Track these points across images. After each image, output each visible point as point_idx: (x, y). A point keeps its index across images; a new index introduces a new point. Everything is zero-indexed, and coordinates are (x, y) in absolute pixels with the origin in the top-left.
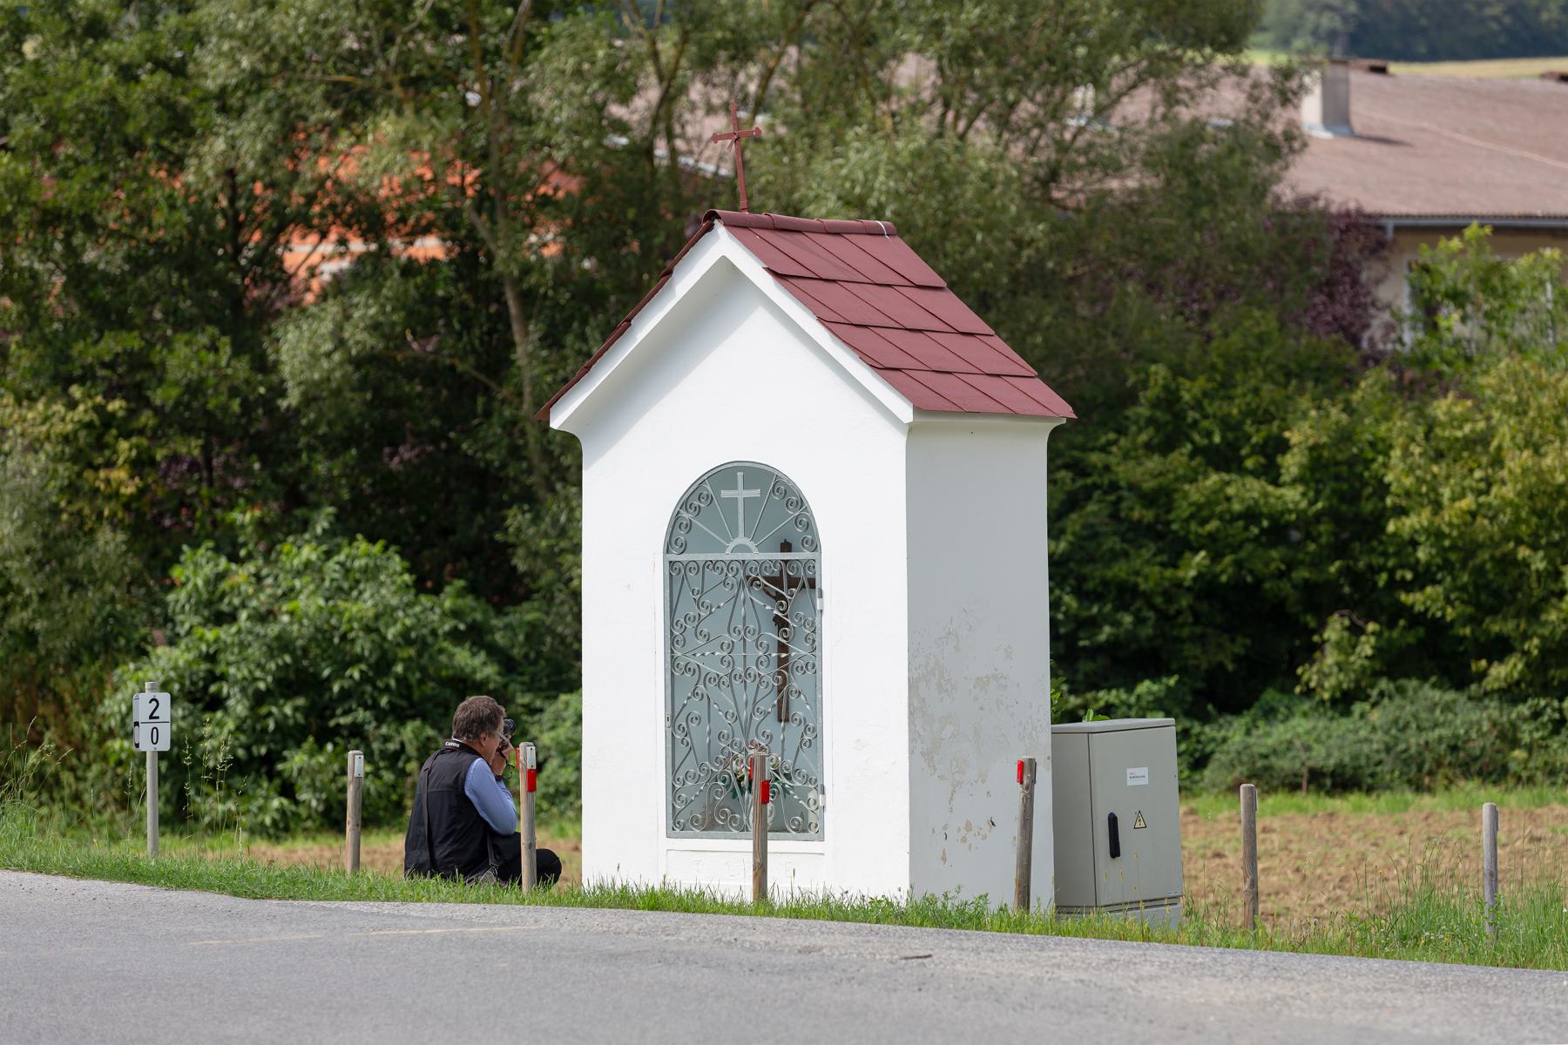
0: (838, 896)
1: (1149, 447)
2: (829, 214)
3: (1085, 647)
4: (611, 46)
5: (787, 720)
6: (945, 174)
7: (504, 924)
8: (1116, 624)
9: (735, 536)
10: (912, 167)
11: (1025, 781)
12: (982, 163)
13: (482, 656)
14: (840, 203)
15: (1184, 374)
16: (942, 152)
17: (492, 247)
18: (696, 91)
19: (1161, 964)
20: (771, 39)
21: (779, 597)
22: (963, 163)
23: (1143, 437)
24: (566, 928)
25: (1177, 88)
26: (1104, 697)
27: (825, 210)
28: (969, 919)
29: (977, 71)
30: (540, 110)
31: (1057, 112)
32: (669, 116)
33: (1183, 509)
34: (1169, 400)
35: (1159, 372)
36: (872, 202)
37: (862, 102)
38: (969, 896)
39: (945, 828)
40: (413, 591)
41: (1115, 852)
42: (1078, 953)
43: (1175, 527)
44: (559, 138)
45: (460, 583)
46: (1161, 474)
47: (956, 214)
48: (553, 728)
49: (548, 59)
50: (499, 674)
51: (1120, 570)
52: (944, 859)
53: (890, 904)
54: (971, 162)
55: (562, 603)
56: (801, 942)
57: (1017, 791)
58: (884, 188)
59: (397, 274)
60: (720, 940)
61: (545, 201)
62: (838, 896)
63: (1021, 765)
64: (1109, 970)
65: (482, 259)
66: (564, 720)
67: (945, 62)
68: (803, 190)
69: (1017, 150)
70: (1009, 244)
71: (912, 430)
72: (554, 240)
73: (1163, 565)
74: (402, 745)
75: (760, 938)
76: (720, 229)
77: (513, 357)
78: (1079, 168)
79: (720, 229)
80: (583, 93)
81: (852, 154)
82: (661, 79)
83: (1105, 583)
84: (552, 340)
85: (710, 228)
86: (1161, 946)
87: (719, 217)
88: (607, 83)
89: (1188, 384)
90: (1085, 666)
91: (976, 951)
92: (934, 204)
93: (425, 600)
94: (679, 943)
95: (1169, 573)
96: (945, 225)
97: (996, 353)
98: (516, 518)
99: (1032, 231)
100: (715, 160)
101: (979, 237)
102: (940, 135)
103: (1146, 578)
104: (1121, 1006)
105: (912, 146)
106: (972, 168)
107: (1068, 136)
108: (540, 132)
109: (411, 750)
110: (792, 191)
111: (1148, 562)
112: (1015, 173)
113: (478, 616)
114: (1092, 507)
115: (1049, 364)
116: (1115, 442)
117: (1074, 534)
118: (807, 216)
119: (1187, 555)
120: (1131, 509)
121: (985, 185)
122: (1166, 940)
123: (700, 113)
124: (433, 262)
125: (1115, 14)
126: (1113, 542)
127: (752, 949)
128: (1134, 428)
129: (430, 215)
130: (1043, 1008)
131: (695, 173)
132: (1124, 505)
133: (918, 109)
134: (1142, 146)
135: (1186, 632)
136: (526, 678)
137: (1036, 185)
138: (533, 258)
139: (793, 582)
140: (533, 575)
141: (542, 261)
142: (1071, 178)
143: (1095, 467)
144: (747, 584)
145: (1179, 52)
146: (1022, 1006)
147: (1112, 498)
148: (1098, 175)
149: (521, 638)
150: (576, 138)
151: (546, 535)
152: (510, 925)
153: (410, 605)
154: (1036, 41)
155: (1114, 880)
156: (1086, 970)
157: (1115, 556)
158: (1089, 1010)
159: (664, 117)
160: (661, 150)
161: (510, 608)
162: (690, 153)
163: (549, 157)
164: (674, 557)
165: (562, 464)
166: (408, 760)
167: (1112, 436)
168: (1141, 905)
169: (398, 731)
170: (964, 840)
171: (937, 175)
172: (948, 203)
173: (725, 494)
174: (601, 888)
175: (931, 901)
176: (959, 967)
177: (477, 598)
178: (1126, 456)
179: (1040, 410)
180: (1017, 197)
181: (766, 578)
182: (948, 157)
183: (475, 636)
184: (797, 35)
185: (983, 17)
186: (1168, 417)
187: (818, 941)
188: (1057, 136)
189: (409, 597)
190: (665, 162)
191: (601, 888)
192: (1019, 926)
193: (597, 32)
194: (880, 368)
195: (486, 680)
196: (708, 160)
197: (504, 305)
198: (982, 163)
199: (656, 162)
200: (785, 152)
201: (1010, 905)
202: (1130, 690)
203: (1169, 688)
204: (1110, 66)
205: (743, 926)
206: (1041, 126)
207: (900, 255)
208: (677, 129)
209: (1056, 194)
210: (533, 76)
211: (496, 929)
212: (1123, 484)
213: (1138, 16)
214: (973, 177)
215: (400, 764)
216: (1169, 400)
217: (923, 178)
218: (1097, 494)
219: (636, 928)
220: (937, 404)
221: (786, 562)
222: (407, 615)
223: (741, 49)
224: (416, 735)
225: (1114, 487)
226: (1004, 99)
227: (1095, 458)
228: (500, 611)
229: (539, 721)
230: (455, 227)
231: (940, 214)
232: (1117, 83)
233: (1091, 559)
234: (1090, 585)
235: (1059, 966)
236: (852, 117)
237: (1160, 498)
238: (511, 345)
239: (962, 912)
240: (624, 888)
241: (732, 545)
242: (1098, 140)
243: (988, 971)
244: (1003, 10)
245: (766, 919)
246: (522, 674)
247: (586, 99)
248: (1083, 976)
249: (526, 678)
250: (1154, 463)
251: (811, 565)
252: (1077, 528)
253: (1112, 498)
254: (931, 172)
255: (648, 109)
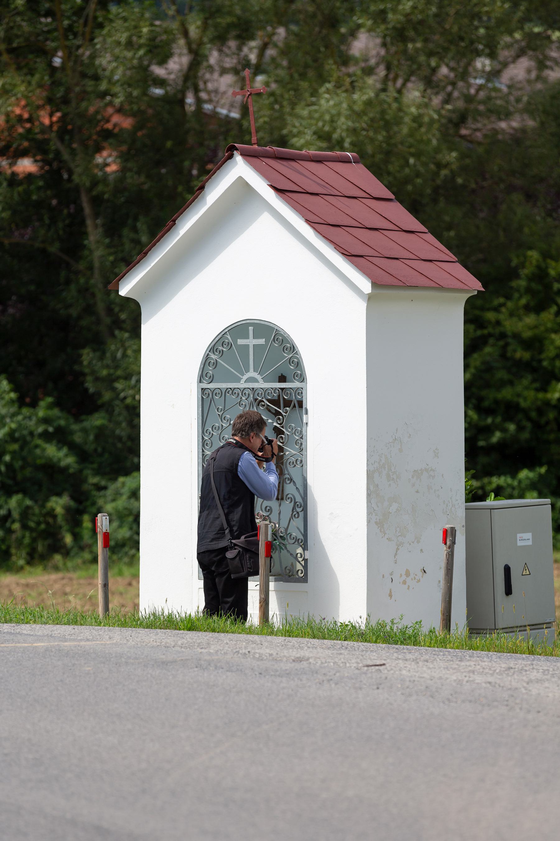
0: (318, 621)
1: (528, 309)
2: (308, 144)
3: (482, 447)
4: (152, 25)
5: (282, 499)
6: (387, 117)
7: (88, 640)
8: (504, 430)
9: (247, 371)
10: (364, 113)
11: (448, 543)
12: (413, 110)
13: (65, 450)
14: (315, 137)
15: (552, 258)
16: (385, 101)
17: (72, 165)
18: (214, 58)
19: (544, 671)
20: (267, 22)
21: (277, 413)
22: (400, 109)
23: (523, 301)
24: (131, 643)
25: (546, 57)
26: (496, 481)
27: (304, 141)
28: (407, 638)
29: (410, 46)
30: (104, 70)
31: (464, 75)
32: (196, 77)
33: (551, 352)
34: (540, 275)
35: (534, 255)
36: (335, 136)
37: (330, 65)
38: (408, 621)
39: (391, 574)
40: (16, 405)
41: (508, 591)
42: (486, 663)
43: (545, 363)
44: (117, 89)
45: (50, 400)
46: (536, 327)
47: (395, 145)
48: (114, 500)
49: (109, 35)
50: (77, 462)
51: (506, 393)
52: (391, 596)
53: (354, 627)
54: (405, 109)
55: (119, 414)
56: (295, 654)
57: (443, 550)
58: (344, 127)
59: (5, 184)
60: (238, 652)
61: (107, 135)
62: (318, 621)
63: (445, 532)
64: (508, 675)
65: (65, 176)
66: (121, 495)
67: (388, 39)
68: (289, 128)
69: (436, 101)
70: (432, 166)
71: (370, 298)
72: (114, 162)
73: (537, 390)
74: (9, 511)
75: (266, 651)
76: (238, 158)
77: (86, 242)
78: (480, 114)
79: (238, 158)
80: (133, 58)
81: (323, 102)
82: (191, 51)
83: (497, 402)
84: (112, 230)
85: (231, 157)
86: (542, 658)
87: (237, 149)
88: (150, 51)
89: (553, 264)
90: (483, 460)
91: (416, 661)
92: (380, 138)
93: (26, 411)
94: (210, 654)
95: (541, 395)
96: (388, 153)
97: (428, 245)
98: (87, 355)
99: (448, 158)
100: (227, 106)
101: (412, 161)
102: (384, 90)
103: (525, 399)
104: (518, 701)
105: (365, 97)
106: (406, 113)
107: (472, 91)
108: (103, 86)
109: (16, 515)
110: (281, 128)
111: (527, 388)
112: (436, 116)
113: (62, 423)
114: (488, 349)
115: (467, 252)
116: (503, 305)
117: (476, 368)
118: (292, 147)
119: (554, 382)
120: (515, 351)
121: (415, 125)
122: (545, 653)
123: (216, 75)
124: (29, 177)
125: (507, 6)
126: (502, 374)
127: (261, 659)
128: (516, 295)
129: (26, 144)
130: (463, 701)
131: (214, 115)
132: (510, 348)
133: (369, 71)
134: (525, 99)
135: (552, 436)
136: (95, 466)
137: (450, 125)
138: (100, 174)
139: (287, 403)
140: (98, 394)
141: (106, 175)
142: (475, 120)
143: (489, 322)
144: (255, 405)
145: (549, 32)
146: (449, 700)
147: (501, 343)
148: (493, 118)
149: (91, 437)
150: (129, 90)
151: (108, 367)
152: (92, 640)
153: (13, 415)
154: (450, 25)
155: (507, 610)
156: (492, 675)
157: (503, 384)
158: (496, 703)
159: (191, 77)
160: (190, 100)
161: (83, 417)
162: (210, 101)
163: (111, 103)
164: (205, 386)
165: (128, 318)
166: (13, 522)
167: (502, 300)
168: (528, 628)
169: (6, 502)
170: (404, 582)
171: (383, 119)
172: (389, 137)
173: (240, 342)
174: (154, 614)
175: (382, 626)
176: (404, 672)
177: (62, 410)
178: (511, 314)
179: (459, 285)
180: (437, 133)
181: (269, 401)
182: (390, 105)
183: (60, 436)
184: (281, 17)
185: (414, 8)
186: (540, 287)
187: (306, 653)
188: (465, 91)
189: (13, 410)
190: (193, 108)
191: (154, 614)
192: (443, 643)
193: (143, 15)
194: (349, 255)
195: (67, 467)
196: (222, 107)
197: (80, 209)
198: (413, 110)
199: (187, 108)
200: (276, 102)
201: (437, 629)
202: (514, 475)
203: (540, 475)
204: (502, 43)
205: (253, 642)
206: (454, 84)
207: (362, 177)
208: (201, 85)
209: (464, 132)
210: (98, 46)
211: (82, 643)
212: (509, 333)
213: (522, 8)
214: (407, 119)
215: (8, 524)
216: (540, 275)
217: (372, 120)
218: (491, 341)
219: (180, 643)
220: (388, 279)
221: (282, 389)
222: (12, 421)
223: (244, 31)
224: (19, 503)
225: (503, 336)
226: (429, 65)
227: (491, 316)
228: (77, 418)
229: (105, 496)
230: (45, 152)
231: (384, 145)
232: (504, 54)
233: (487, 385)
234: (486, 404)
235: (473, 672)
236: (322, 79)
237: (535, 344)
238: (85, 234)
239: (404, 633)
240: (170, 615)
241: (245, 378)
242: (493, 94)
243: (425, 675)
244: (429, 2)
245: (269, 638)
246: (92, 463)
247: (135, 62)
248: (490, 679)
249: (95, 466)
250: (530, 319)
251: (300, 392)
252: (478, 363)
253: (501, 343)
254: (378, 116)
255: (181, 70)
